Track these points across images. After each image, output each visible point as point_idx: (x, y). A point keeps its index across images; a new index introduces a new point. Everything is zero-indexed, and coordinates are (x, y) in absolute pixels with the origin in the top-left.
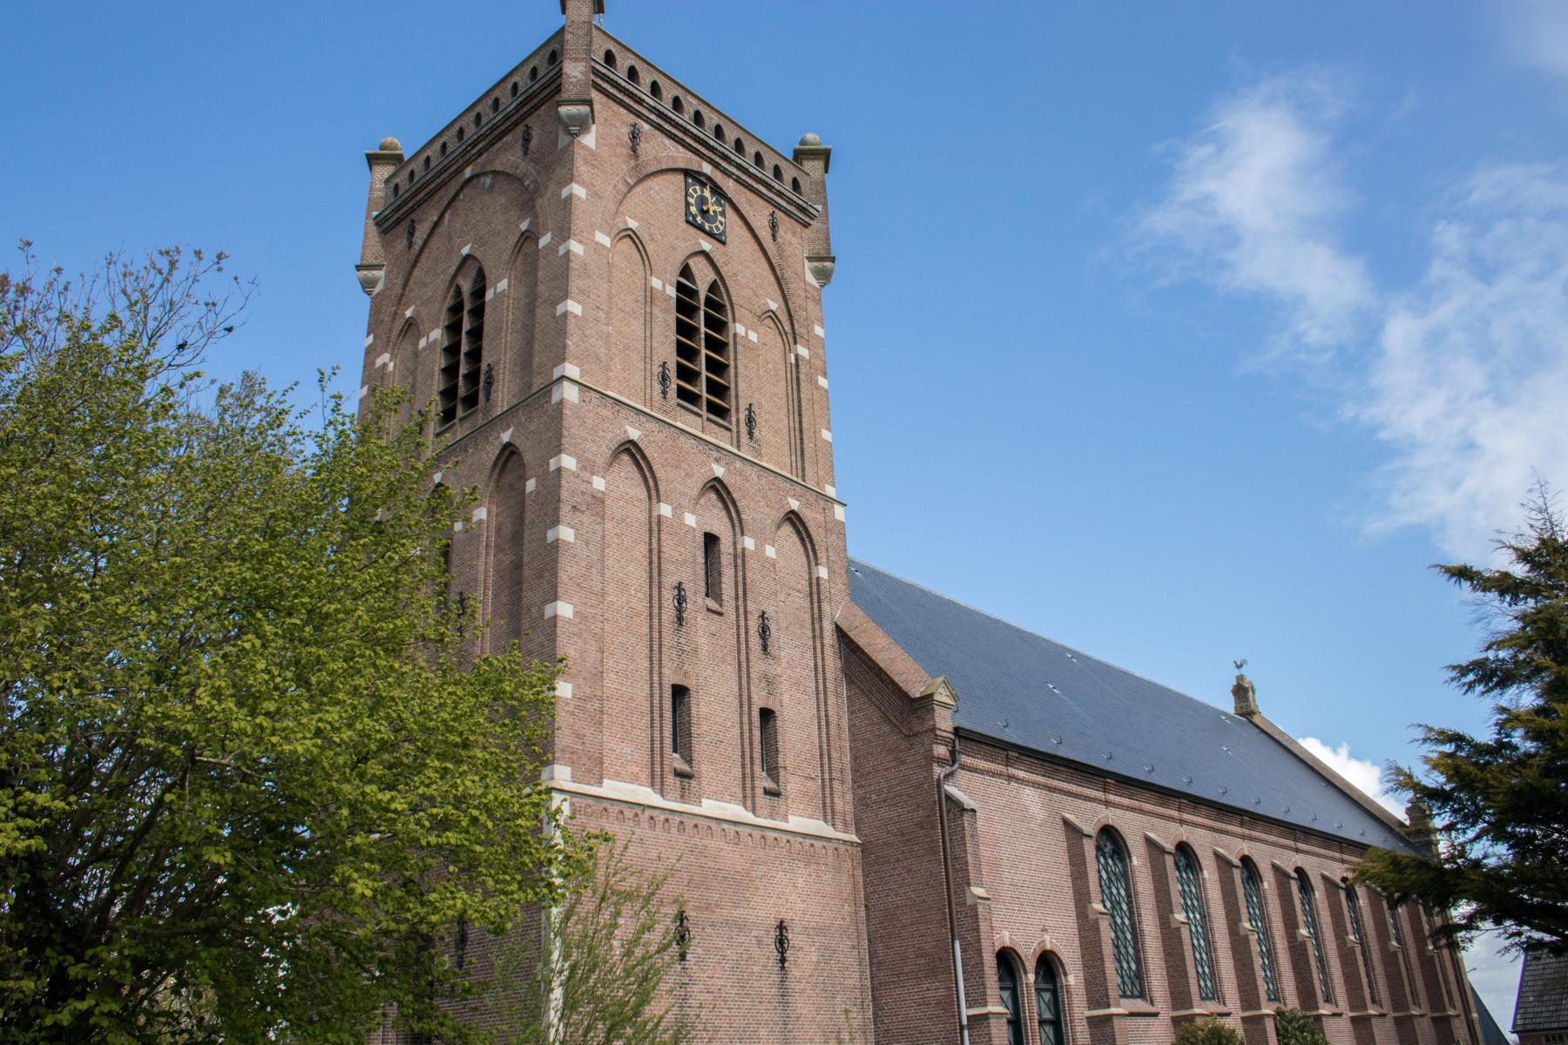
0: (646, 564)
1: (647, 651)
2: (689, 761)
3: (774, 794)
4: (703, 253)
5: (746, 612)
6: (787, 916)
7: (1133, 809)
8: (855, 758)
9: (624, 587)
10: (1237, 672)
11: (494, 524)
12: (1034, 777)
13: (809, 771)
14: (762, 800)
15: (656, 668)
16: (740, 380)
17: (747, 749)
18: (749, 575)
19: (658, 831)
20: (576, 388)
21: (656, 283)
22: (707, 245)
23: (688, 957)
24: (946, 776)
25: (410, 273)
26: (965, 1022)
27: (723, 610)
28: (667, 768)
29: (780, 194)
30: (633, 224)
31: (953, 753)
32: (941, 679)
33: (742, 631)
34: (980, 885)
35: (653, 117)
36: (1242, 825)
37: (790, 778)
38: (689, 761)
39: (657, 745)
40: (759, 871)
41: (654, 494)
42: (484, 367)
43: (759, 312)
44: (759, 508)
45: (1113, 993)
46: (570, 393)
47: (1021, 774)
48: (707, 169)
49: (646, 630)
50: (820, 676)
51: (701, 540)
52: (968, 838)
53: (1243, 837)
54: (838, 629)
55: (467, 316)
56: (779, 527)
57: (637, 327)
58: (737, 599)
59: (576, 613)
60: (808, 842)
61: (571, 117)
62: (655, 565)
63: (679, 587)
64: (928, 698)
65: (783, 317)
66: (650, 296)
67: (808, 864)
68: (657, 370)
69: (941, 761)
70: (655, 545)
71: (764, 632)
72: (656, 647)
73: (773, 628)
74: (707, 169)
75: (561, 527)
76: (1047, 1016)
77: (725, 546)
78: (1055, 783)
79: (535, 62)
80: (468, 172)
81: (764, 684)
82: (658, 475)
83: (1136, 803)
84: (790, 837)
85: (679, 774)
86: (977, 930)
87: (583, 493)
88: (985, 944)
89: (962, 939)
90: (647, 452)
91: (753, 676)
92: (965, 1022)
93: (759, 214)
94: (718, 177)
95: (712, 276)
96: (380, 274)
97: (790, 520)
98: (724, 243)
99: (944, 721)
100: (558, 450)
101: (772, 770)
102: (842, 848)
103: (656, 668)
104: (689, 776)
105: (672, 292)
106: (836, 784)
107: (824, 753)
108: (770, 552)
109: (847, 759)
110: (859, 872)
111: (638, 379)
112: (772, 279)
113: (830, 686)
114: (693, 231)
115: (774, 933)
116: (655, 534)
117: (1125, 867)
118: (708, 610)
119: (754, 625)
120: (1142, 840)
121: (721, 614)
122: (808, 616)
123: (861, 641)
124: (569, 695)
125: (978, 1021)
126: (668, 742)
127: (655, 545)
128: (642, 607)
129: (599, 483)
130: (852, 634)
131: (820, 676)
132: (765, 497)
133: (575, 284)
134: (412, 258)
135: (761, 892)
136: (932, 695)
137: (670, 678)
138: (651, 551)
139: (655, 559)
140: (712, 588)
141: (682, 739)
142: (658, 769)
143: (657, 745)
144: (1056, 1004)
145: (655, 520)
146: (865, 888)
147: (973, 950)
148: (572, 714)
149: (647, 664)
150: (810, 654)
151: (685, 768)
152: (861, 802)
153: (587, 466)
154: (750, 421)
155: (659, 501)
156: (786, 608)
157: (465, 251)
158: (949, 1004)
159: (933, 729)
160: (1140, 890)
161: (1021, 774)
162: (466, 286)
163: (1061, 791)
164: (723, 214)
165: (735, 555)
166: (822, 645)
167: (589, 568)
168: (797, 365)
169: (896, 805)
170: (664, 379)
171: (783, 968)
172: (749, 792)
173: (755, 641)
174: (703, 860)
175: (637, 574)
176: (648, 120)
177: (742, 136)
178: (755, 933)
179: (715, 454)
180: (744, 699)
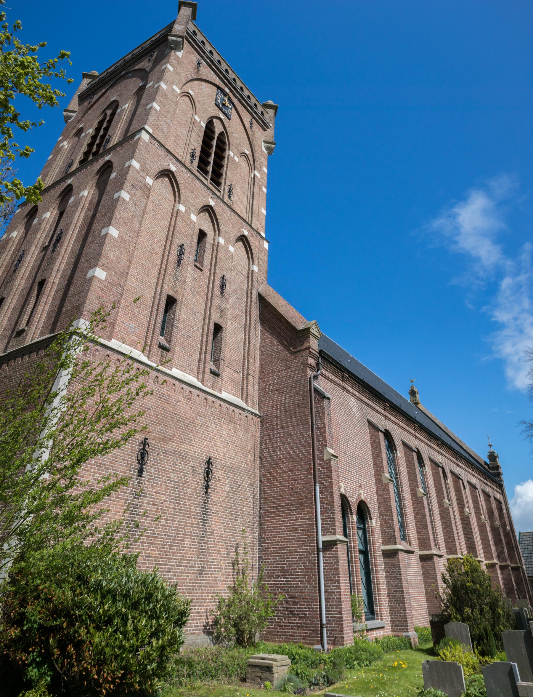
0: (166, 230)
1: (157, 274)
2: (169, 342)
3: (216, 374)
4: (219, 119)
5: (215, 273)
6: (214, 455)
7: (396, 424)
8: (262, 365)
9: (151, 236)
10: (411, 384)
11: (89, 199)
13: (236, 368)
14: (209, 377)
15: (160, 284)
16: (228, 173)
17: (204, 343)
18: (219, 255)
20: (148, 136)
21: (197, 118)
22: (222, 116)
23: (144, 474)
25: (87, 112)
26: (321, 546)
27: (203, 269)
28: (154, 341)
32: (314, 321)
33: (211, 282)
35: (208, 60)
36: (438, 446)
37: (226, 369)
38: (169, 342)
39: (152, 326)
40: (200, 421)
41: (177, 199)
45: (398, 540)
46: (144, 136)
48: (227, 90)
49: (159, 262)
50: (248, 317)
51: (197, 231)
52: (326, 415)
53: (439, 452)
54: (260, 296)
57: (185, 131)
58: (211, 265)
59: (119, 236)
60: (232, 408)
61: (173, 41)
62: (171, 232)
63: (182, 246)
64: (306, 331)
66: (193, 122)
67: (230, 422)
68: (190, 150)
70: (173, 223)
71: (223, 285)
72: (162, 273)
73: (228, 285)
74: (227, 90)
75: (123, 191)
76: (362, 548)
80: (123, 73)
81: (218, 311)
82: (181, 191)
83: (397, 421)
84: (222, 403)
86: (330, 477)
87: (139, 181)
88: (335, 488)
89: (321, 483)
90: (178, 179)
91: (213, 304)
92: (321, 546)
93: (247, 118)
95: (222, 129)
96: (75, 114)
98: (230, 119)
99: (314, 344)
101: (217, 361)
102: (250, 417)
103: (160, 284)
104: (167, 350)
105: (204, 125)
106: (250, 378)
107: (246, 359)
109: (257, 365)
110: (258, 434)
112: (248, 142)
113: (253, 323)
115: (204, 466)
116: (174, 218)
117: (394, 456)
120: (401, 443)
121: (201, 270)
122: (245, 287)
123: (272, 301)
124: (103, 279)
125: (329, 545)
126: (159, 325)
127: (173, 223)
128: (160, 250)
129: (149, 181)
130: (267, 298)
131: (248, 317)
132: (232, 224)
133: (158, 97)
134: (89, 106)
135: (200, 435)
137: (168, 290)
138: (170, 225)
139: (171, 229)
141: (166, 327)
142: (149, 341)
143: (152, 326)
144: (365, 540)
145: (175, 211)
146: (261, 445)
147: (328, 490)
148: (102, 290)
149: (156, 281)
150: (244, 305)
151: (166, 344)
152: (263, 391)
153: (144, 169)
154: (230, 191)
155: (179, 203)
158: (311, 530)
159: (309, 348)
160: (402, 471)
161: (349, 388)
164: (231, 109)
165: (214, 245)
166: (251, 301)
167: (134, 217)
168: (254, 178)
169: (284, 392)
171: (206, 493)
172: (201, 369)
173: (217, 289)
174: (166, 405)
175: (161, 235)
178: (192, 464)
179: (211, 195)
180: (207, 316)
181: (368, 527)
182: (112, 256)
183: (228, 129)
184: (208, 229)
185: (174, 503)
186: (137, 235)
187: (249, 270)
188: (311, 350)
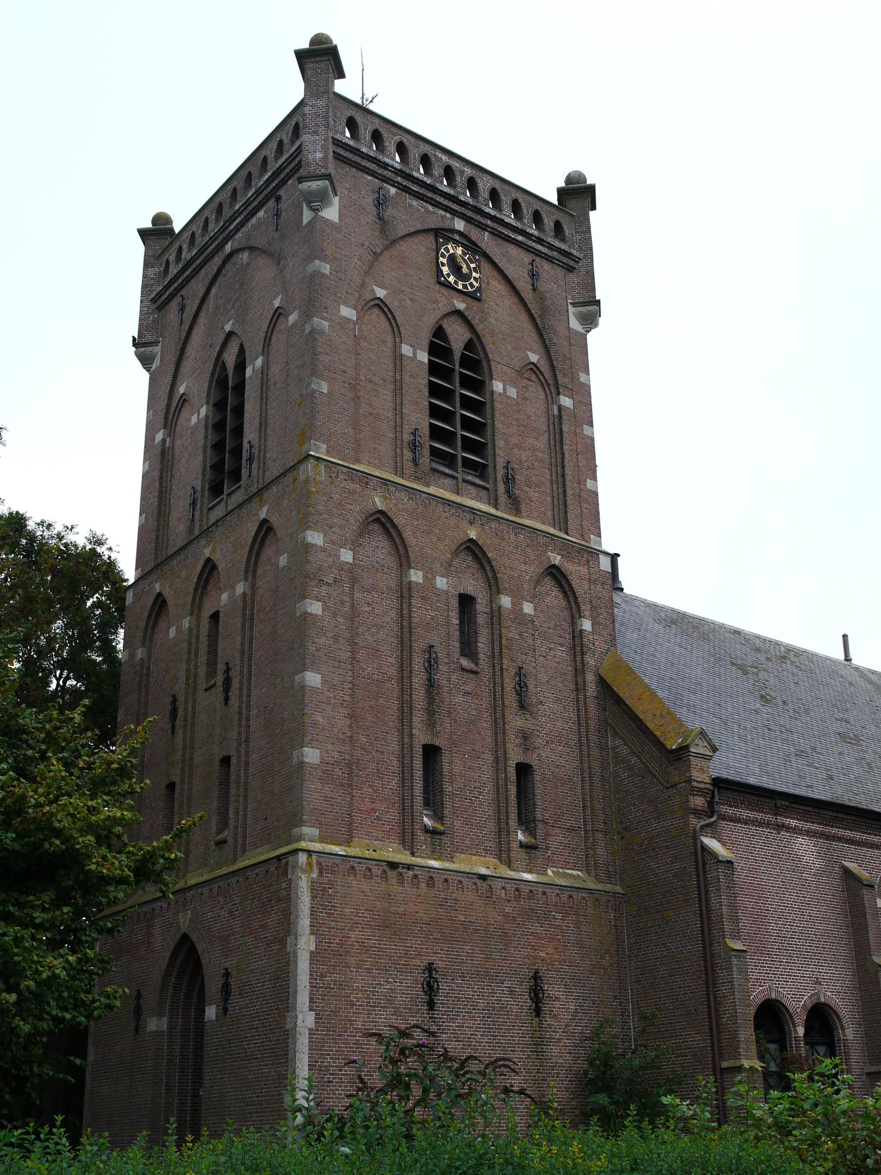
4: (458, 313)
12: (808, 826)
19: (407, 887)
24: (702, 827)
29: (540, 241)
30: (381, 293)
31: (711, 804)
34: (737, 936)
42: (246, 445)
43: (518, 365)
44: (517, 564)
47: (794, 823)
51: (455, 603)
54: (602, 682)
55: (228, 393)
56: (538, 582)
59: (324, 682)
65: (544, 367)
69: (697, 813)
71: (521, 689)
73: (531, 684)
74: (460, 225)
77: (481, 606)
78: (834, 831)
79: (206, 213)
80: (228, 248)
85: (434, 832)
93: (515, 263)
94: (475, 234)
97: (551, 574)
98: (479, 300)
100: (305, 524)
105: (423, 357)
108: (528, 608)
111: (385, 448)
114: (445, 291)
118: (463, 669)
119: (509, 684)
121: (476, 673)
124: (317, 761)
136: (687, 747)
140: (468, 648)
156: (547, 666)
157: (228, 328)
159: (689, 780)
162: (230, 359)
163: (840, 839)
168: (560, 417)
170: (414, 446)
173: (511, 700)
174: (453, 913)
176: (394, 184)
177: (498, 185)
181: (839, 1040)
182: (321, 719)
183: (479, 328)
184: (473, 585)
185: (487, 1036)
186: (350, 667)
187: (573, 632)
188: (694, 784)
